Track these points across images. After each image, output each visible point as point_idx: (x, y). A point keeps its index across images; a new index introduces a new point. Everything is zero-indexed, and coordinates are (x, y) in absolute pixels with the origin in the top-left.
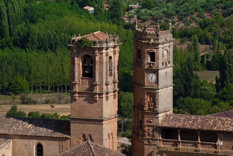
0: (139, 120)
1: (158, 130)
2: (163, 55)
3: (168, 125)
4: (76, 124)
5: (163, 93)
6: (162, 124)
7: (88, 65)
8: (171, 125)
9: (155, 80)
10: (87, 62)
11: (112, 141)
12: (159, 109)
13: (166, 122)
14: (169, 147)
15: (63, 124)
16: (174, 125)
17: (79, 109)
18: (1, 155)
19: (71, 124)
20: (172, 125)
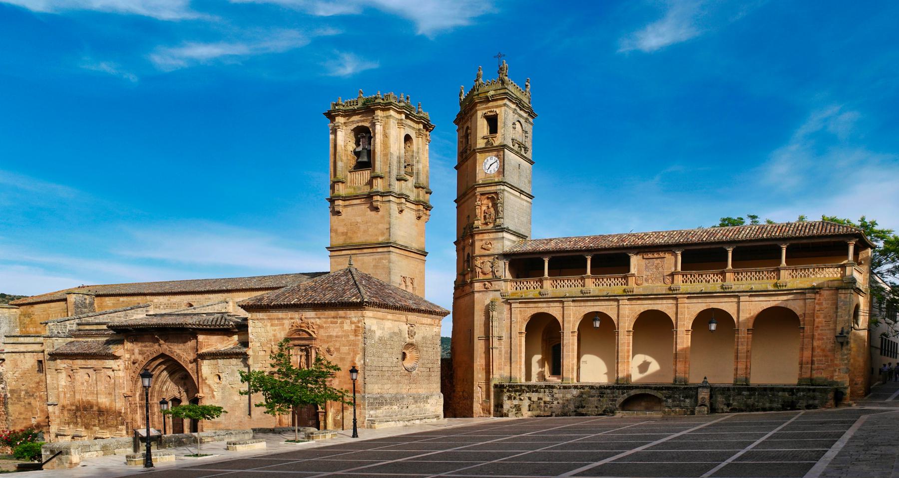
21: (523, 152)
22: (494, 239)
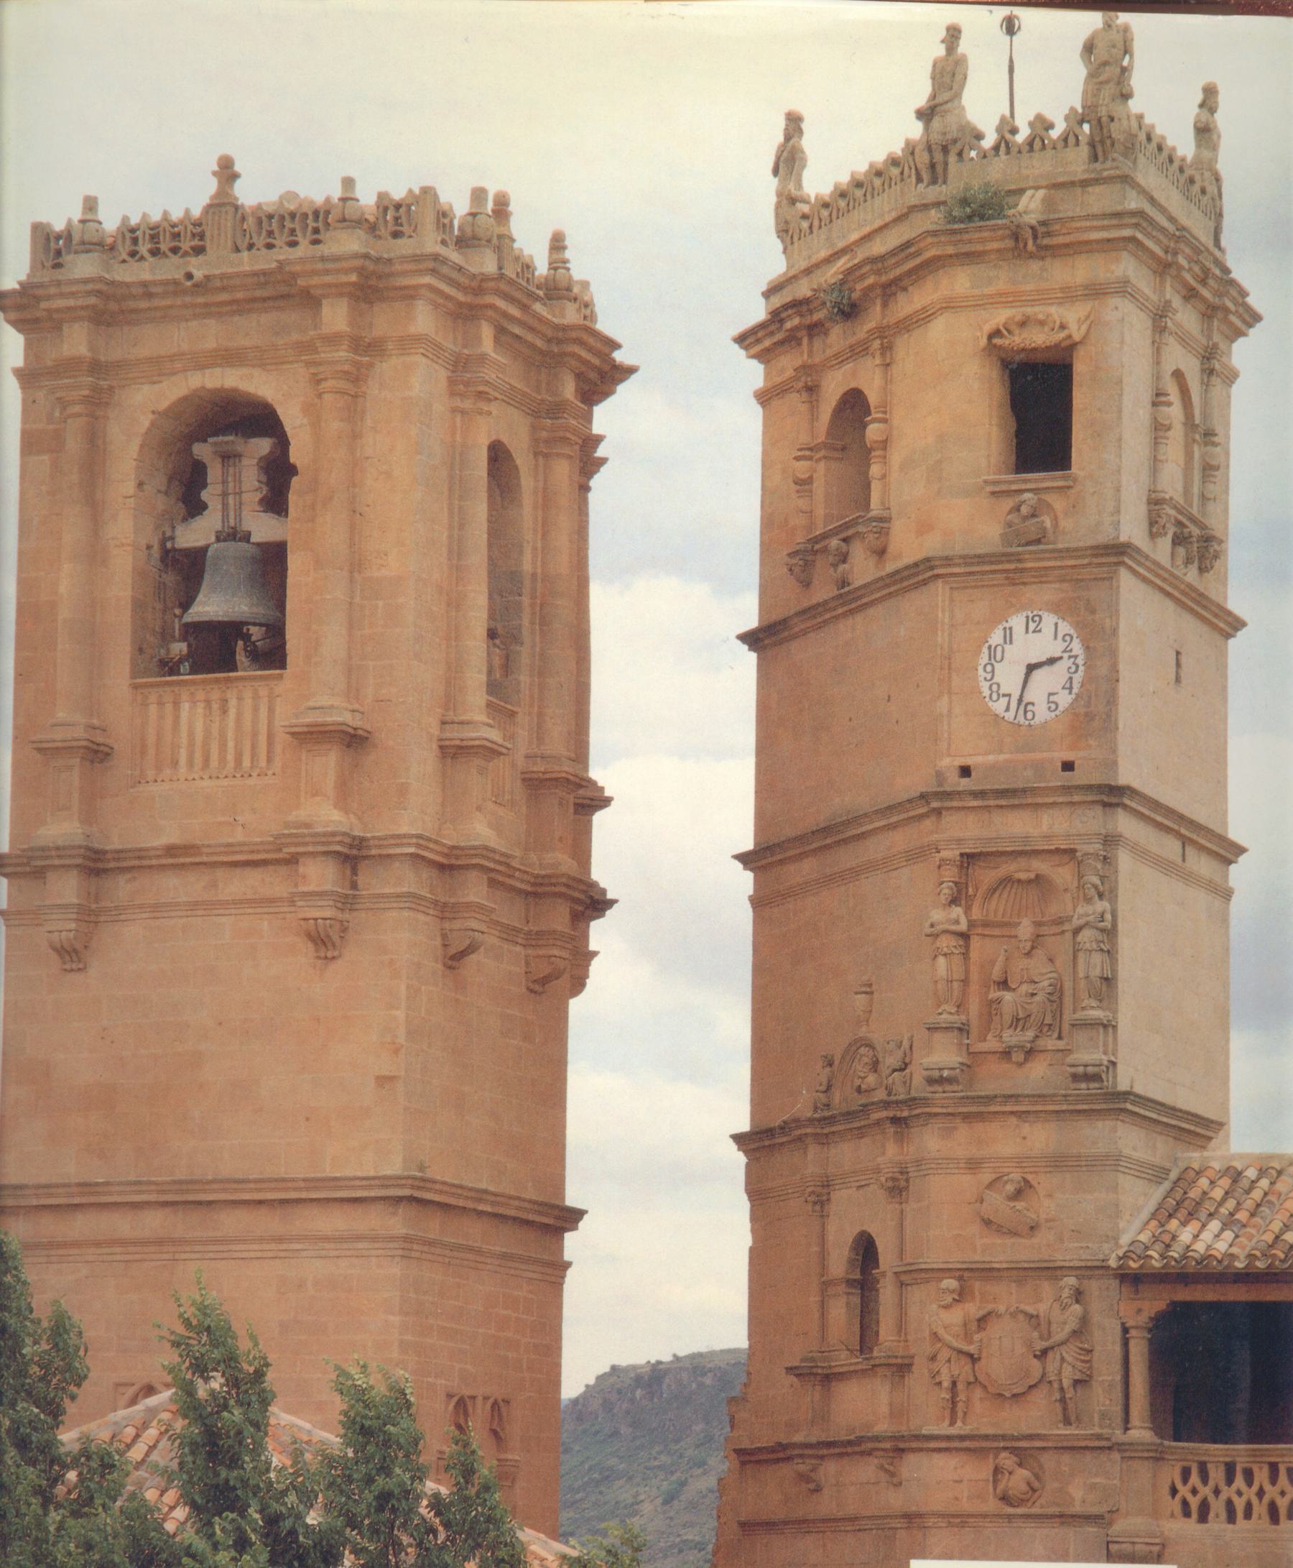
7: (234, 535)
21: (1191, 575)
22: (1058, 1162)
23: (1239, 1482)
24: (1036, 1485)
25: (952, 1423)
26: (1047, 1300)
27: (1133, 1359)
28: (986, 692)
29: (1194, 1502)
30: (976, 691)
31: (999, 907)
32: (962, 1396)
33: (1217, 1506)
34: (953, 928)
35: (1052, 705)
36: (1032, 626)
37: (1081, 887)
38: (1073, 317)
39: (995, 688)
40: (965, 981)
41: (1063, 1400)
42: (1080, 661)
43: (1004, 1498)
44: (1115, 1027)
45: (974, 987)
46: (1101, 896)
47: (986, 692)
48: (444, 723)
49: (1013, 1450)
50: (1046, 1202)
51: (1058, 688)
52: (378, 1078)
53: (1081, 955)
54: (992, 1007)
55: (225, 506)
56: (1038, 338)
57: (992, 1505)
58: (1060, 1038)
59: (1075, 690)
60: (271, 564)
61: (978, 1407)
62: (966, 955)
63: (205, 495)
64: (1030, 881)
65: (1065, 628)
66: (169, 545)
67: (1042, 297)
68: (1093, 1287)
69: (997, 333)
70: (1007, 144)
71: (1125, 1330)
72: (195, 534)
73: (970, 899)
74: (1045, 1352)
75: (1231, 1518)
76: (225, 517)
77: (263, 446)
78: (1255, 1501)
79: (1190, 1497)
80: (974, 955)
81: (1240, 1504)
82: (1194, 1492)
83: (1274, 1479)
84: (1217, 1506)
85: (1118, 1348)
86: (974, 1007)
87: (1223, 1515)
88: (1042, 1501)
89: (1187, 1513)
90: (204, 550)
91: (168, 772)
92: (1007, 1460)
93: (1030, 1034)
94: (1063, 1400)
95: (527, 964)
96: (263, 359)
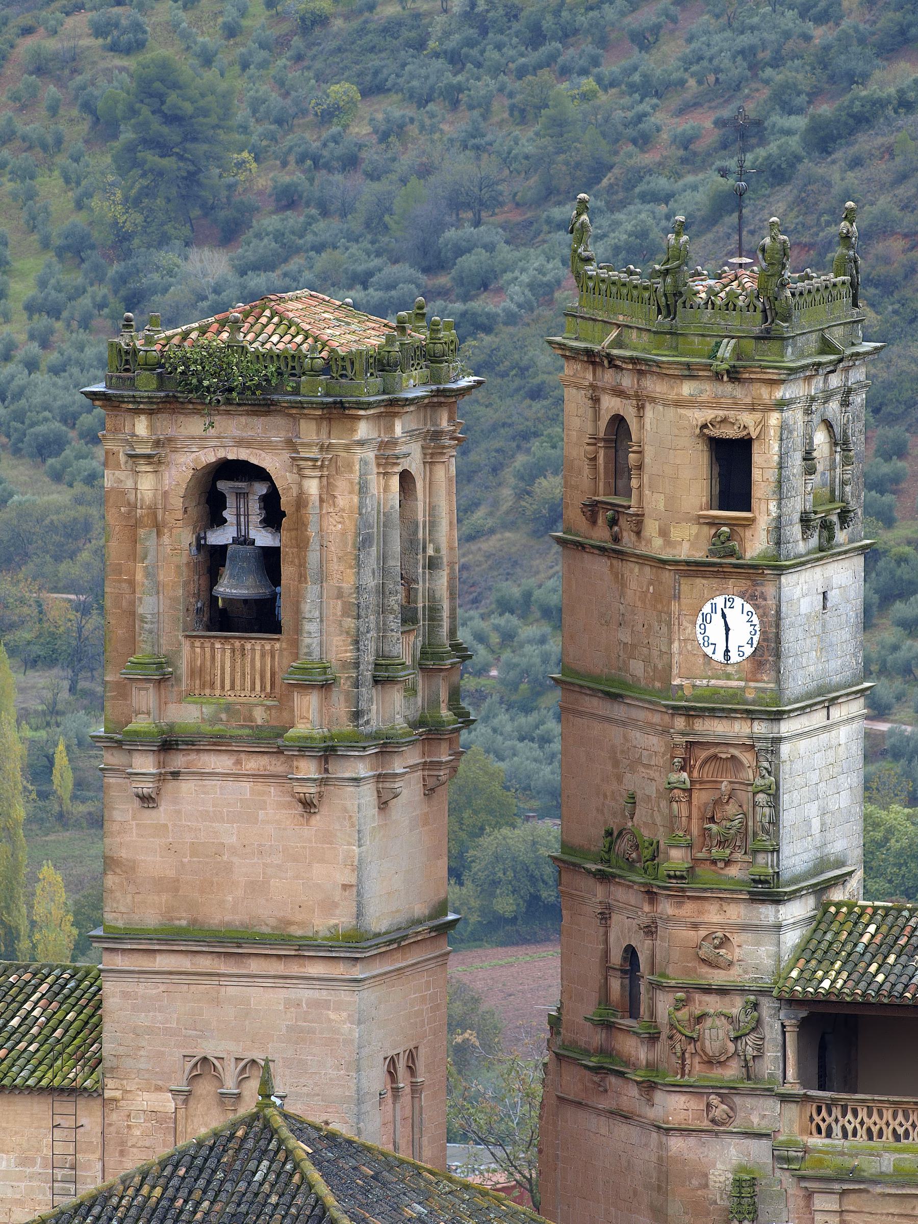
0: (616, 957)
1: (777, 1026)
2: (808, 457)
3: (850, 984)
4: (147, 989)
5: (803, 745)
6: (807, 978)
7: (243, 540)
8: (874, 986)
9: (748, 651)
10: (228, 514)
11: (408, 1113)
12: (784, 863)
13: (838, 965)
14: (15, 766)
15: (29, 989)
16: (900, 987)
17: (171, 873)
18: (877, 1135)
19: (111, 989)
20: (887, 986)
22: (744, 928)
23: (849, 1116)
24: (731, 1114)
25: (683, 1076)
26: (736, 1006)
27: (788, 1044)
28: (701, 642)
29: (823, 1126)
30: (695, 640)
31: (708, 773)
32: (688, 1061)
33: (837, 1130)
34: (682, 786)
35: (741, 653)
36: (728, 604)
37: (758, 767)
38: (748, 419)
39: (707, 639)
40: (689, 817)
41: (746, 1066)
42: (758, 628)
43: (713, 1121)
44: (778, 851)
45: (694, 821)
46: (769, 773)
47: (701, 642)
48: (376, 665)
49: (717, 1094)
50: (737, 950)
51: (744, 644)
52: (343, 885)
53: (758, 809)
54: (705, 832)
55: (238, 524)
56: (730, 433)
57: (706, 1124)
58: (745, 853)
59: (755, 645)
60: (270, 561)
61: (697, 1067)
62: (690, 802)
63: (225, 514)
64: (727, 758)
65: (748, 607)
66: (202, 542)
67: (736, 404)
68: (767, 1006)
69: (705, 426)
70: (713, 304)
71: (783, 1026)
72: (221, 537)
73: (692, 767)
74: (737, 1038)
75: (845, 1135)
76: (239, 530)
77: (261, 489)
78: (858, 1127)
79: (821, 1123)
80: (695, 802)
81: (850, 1128)
82: (824, 1120)
83: (870, 1116)
84: (837, 1130)
85: (780, 1038)
86: (695, 830)
87: (840, 1135)
88: (735, 1124)
89: (819, 1131)
90: (224, 547)
91: (207, 691)
92: (714, 1100)
93: (728, 851)
94: (746, 1066)
95: (424, 780)
96: (264, 445)
